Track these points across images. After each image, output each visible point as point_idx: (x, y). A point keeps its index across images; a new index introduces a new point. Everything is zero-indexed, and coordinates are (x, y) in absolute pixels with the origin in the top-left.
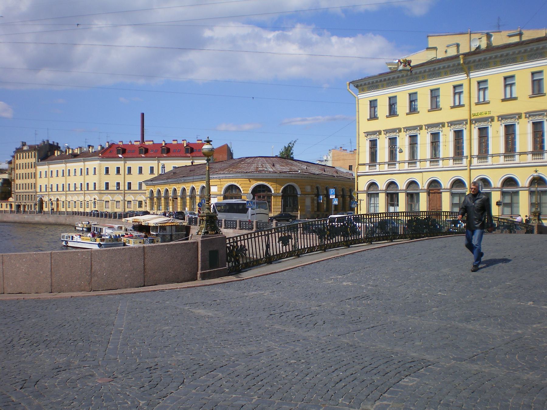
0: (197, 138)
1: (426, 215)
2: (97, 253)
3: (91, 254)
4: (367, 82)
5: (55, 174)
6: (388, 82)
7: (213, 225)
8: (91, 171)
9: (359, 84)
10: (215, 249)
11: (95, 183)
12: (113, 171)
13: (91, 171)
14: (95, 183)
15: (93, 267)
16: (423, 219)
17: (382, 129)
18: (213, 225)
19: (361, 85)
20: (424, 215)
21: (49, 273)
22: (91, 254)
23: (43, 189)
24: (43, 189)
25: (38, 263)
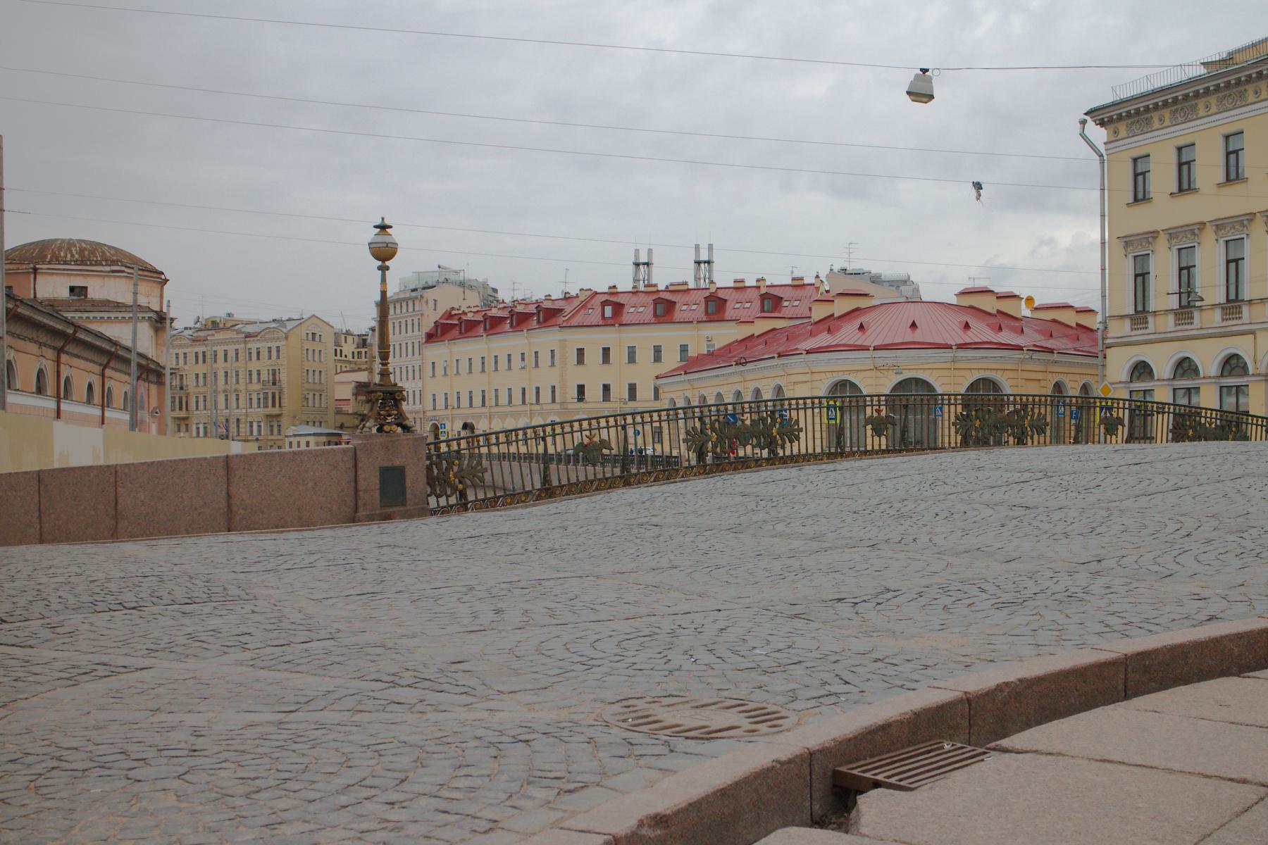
0: (792, 272)
1: (1221, 420)
2: (126, 470)
3: (116, 472)
4: (1123, 111)
5: (464, 366)
6: (1173, 108)
7: (396, 412)
8: (545, 359)
9: (1105, 116)
10: (397, 463)
11: (553, 388)
12: (593, 356)
13: (545, 359)
14: (553, 388)
15: (120, 501)
16: (1213, 426)
17: (1205, 220)
18: (396, 412)
19: (1111, 120)
20: (1216, 419)
21: (37, 514)
22: (116, 472)
23: (441, 403)
24: (441, 403)
25: (14, 493)
